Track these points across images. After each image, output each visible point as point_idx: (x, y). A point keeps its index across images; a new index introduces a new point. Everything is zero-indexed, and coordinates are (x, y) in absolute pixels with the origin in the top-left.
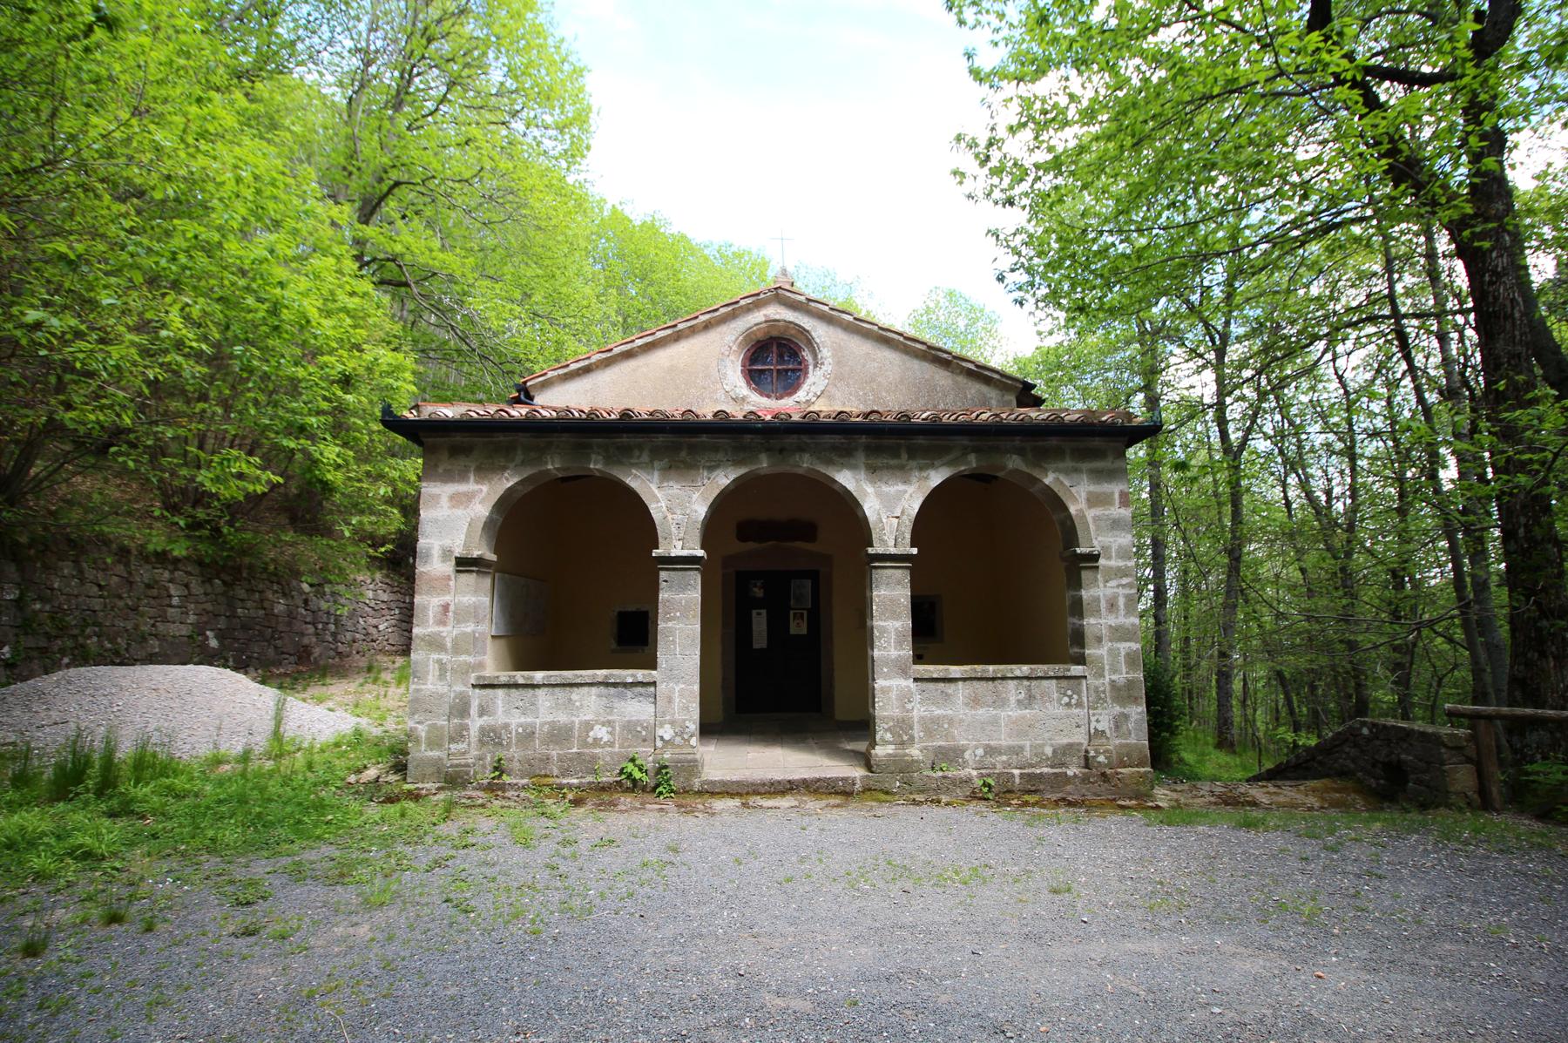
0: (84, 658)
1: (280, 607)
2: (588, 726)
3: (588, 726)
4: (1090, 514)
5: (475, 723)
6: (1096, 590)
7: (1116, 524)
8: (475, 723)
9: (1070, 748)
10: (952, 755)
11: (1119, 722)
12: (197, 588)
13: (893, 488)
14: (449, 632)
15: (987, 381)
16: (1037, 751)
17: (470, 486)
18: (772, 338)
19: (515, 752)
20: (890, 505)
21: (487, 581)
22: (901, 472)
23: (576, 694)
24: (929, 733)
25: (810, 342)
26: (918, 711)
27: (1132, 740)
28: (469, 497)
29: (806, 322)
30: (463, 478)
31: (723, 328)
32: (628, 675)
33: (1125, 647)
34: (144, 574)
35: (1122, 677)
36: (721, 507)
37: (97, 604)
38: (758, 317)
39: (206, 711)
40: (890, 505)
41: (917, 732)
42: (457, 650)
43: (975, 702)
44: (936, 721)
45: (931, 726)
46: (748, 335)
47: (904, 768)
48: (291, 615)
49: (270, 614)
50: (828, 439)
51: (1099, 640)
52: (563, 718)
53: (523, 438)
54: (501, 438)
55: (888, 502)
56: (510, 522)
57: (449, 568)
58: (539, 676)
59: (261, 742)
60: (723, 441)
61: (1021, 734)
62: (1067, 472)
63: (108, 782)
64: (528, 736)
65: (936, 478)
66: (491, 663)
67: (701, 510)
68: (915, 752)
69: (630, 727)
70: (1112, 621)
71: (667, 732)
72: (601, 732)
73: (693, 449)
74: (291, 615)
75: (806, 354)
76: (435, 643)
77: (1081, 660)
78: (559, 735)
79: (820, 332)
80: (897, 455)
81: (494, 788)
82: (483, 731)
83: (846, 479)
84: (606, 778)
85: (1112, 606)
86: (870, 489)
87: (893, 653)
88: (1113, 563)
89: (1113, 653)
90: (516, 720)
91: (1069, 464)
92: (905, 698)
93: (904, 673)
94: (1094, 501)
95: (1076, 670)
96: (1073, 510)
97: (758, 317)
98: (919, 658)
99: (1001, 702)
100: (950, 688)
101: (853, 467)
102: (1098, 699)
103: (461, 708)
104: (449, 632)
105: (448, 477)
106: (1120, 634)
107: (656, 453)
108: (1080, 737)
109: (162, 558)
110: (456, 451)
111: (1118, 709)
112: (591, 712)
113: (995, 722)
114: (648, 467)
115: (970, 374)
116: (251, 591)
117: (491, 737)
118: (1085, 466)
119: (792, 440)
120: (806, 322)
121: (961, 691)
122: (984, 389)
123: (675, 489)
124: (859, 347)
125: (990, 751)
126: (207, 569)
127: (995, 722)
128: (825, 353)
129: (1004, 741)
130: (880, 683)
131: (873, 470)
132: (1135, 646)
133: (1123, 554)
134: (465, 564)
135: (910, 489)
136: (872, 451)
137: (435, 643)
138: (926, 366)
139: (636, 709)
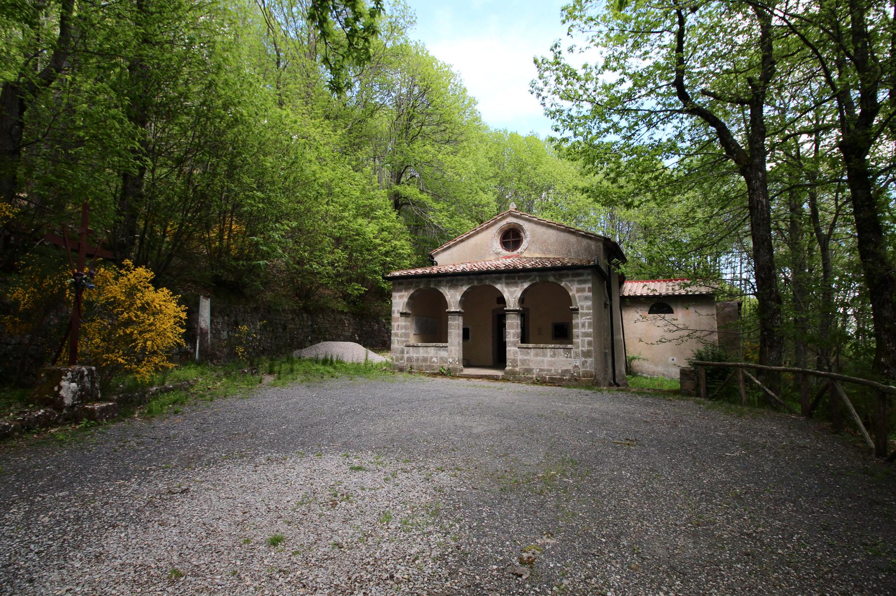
0: (326, 340)
1: (376, 327)
2: (432, 358)
3: (432, 358)
4: (577, 295)
5: (406, 356)
6: (578, 321)
7: (586, 298)
8: (406, 356)
9: (567, 371)
10: (529, 371)
11: (584, 363)
12: (352, 321)
13: (513, 289)
14: (399, 332)
15: (590, 238)
16: (556, 371)
17: (403, 293)
18: (510, 229)
19: (414, 363)
20: (512, 294)
21: (409, 319)
22: (516, 284)
23: (429, 349)
24: (523, 364)
25: (523, 229)
26: (519, 357)
27: (588, 369)
28: (403, 296)
29: (521, 222)
30: (401, 291)
31: (492, 228)
32: (441, 345)
33: (587, 339)
34: (338, 317)
35: (585, 349)
36: (465, 295)
37: (328, 326)
38: (504, 222)
39: (352, 352)
40: (512, 294)
41: (519, 363)
42: (401, 337)
43: (537, 355)
44: (525, 360)
45: (523, 362)
46: (501, 229)
47: (513, 373)
48: (380, 330)
49: (373, 330)
50: (494, 275)
51: (578, 336)
52: (425, 355)
53: (415, 280)
54: (410, 280)
55: (511, 293)
56: (412, 302)
57: (399, 315)
58: (431, 344)
59: (363, 361)
60: (465, 278)
61: (551, 365)
62: (570, 281)
63: (332, 363)
64: (418, 359)
65: (526, 285)
66: (413, 340)
67: (459, 298)
68: (517, 369)
69: (442, 358)
70: (583, 330)
71: (451, 360)
72: (435, 359)
73: (457, 280)
74: (380, 330)
75: (522, 234)
76: (396, 335)
77: (572, 343)
78: (425, 360)
79: (526, 225)
80: (514, 278)
81: (410, 372)
82: (408, 358)
83: (498, 287)
84: (436, 371)
85: (583, 325)
86: (506, 290)
87: (512, 340)
88: (585, 311)
89: (583, 341)
90: (415, 355)
91: (570, 278)
92: (515, 353)
93: (515, 346)
94: (578, 290)
95: (570, 346)
96: (570, 294)
97: (504, 222)
98: (523, 341)
99: (545, 355)
100: (529, 351)
101: (501, 283)
102: (577, 355)
103: (402, 352)
104: (399, 332)
105: (399, 291)
106: (586, 335)
107: (447, 282)
108: (570, 367)
109: (342, 312)
110: (400, 284)
111: (584, 359)
112: (432, 354)
113: (543, 361)
114: (445, 286)
115: (583, 236)
116: (367, 322)
117: (410, 359)
118: (576, 279)
119: (483, 276)
120: (521, 222)
121: (532, 352)
122: (589, 241)
123: (452, 291)
124: (540, 230)
125: (541, 370)
126: (354, 315)
127: (543, 361)
128: (528, 233)
129: (546, 368)
130: (508, 348)
131: (507, 284)
132: (590, 339)
133: (588, 308)
134: (402, 314)
135: (518, 289)
136: (507, 278)
137: (396, 335)
138: (566, 234)
139: (443, 354)
